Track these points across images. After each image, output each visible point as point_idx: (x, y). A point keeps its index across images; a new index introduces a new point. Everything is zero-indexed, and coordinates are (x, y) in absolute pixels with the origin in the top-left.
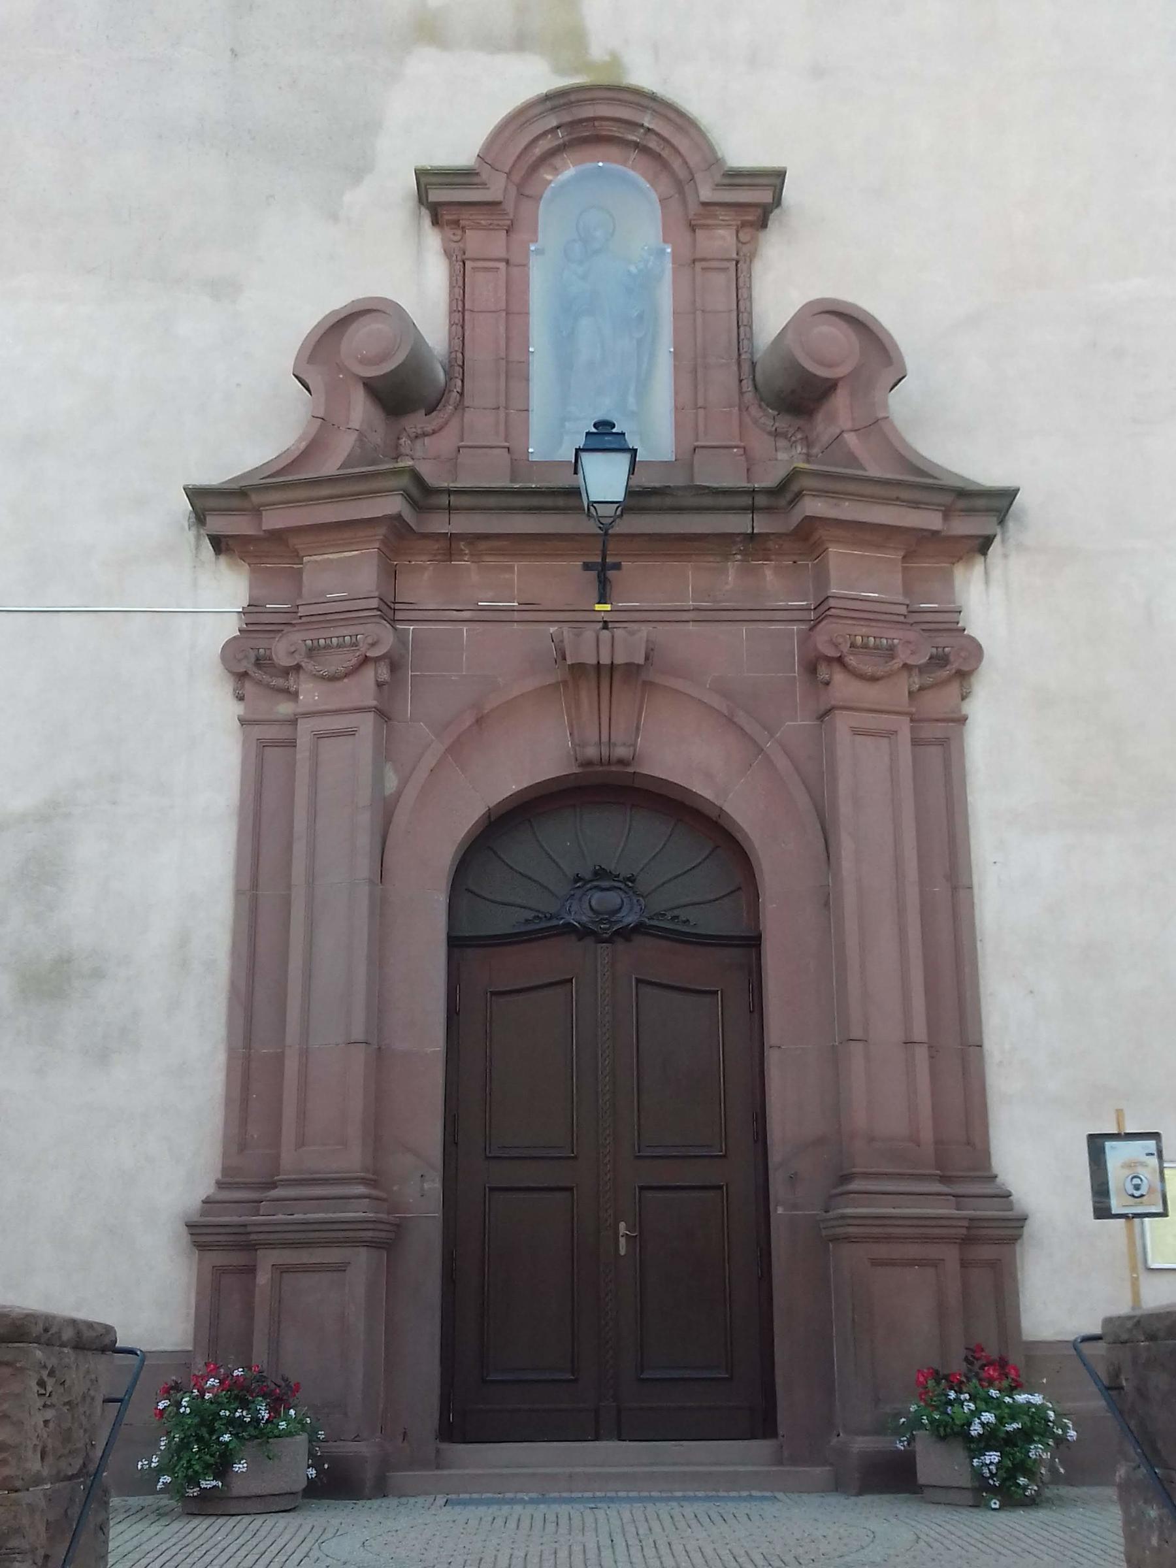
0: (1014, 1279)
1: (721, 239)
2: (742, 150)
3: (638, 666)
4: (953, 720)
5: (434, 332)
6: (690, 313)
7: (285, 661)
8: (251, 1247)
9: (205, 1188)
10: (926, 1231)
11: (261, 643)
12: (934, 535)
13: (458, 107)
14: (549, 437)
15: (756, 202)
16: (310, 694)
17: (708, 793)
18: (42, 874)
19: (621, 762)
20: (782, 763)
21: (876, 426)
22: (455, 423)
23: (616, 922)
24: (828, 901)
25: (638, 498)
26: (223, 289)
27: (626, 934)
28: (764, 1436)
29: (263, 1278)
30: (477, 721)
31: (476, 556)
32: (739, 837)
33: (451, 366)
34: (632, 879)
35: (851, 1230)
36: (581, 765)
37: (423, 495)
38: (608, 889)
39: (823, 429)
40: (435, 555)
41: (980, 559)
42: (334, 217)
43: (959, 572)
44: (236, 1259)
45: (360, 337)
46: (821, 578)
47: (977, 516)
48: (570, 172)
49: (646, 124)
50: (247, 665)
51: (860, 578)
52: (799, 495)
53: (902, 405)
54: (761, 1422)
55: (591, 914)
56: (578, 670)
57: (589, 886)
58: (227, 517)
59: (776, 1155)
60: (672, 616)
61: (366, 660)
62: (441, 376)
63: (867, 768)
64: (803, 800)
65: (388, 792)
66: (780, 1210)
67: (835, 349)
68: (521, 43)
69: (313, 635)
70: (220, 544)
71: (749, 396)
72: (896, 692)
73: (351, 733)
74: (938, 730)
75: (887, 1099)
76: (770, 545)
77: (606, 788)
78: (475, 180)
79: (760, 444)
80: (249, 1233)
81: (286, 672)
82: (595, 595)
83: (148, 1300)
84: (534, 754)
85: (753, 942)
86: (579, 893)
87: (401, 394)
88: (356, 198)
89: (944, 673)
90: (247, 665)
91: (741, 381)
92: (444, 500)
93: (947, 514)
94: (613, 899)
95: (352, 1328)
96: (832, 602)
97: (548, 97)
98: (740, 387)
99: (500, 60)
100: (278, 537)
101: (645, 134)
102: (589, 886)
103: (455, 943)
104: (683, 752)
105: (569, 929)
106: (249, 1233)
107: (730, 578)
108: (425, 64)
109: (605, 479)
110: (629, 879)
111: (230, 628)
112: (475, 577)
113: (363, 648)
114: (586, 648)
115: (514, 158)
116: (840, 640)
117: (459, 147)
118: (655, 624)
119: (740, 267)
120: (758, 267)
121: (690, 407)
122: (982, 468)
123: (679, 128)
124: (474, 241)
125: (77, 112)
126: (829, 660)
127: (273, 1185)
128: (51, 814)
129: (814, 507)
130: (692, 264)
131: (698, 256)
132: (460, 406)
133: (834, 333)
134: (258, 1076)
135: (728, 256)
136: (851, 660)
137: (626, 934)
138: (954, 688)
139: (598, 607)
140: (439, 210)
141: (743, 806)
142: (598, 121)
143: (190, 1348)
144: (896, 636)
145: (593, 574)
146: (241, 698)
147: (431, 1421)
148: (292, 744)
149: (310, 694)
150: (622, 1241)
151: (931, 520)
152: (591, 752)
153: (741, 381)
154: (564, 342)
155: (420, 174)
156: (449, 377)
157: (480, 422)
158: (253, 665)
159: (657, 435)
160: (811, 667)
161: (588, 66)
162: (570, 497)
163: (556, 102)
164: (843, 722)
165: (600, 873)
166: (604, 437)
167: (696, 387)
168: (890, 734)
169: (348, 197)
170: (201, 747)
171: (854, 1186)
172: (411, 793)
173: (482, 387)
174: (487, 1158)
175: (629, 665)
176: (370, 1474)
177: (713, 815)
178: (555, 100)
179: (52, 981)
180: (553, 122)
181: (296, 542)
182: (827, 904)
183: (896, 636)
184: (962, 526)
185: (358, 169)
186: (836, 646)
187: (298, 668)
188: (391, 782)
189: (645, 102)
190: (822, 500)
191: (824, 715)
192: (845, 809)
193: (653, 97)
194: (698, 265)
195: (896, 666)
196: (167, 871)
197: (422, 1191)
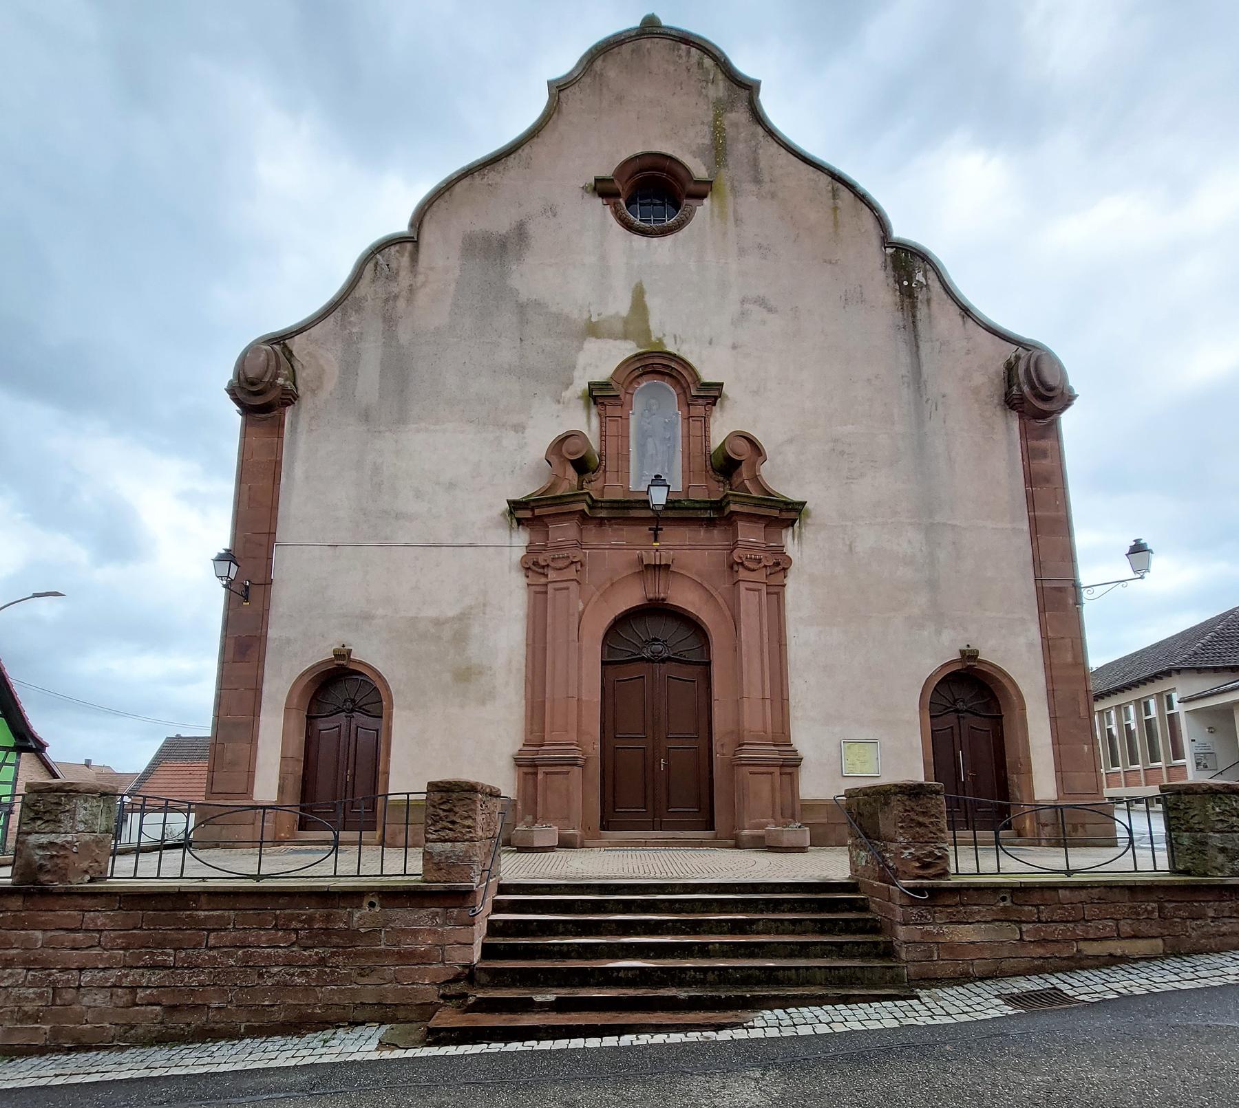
1: (698, 410)
2: (707, 376)
5: (595, 445)
6: (687, 436)
8: (536, 766)
9: (520, 747)
10: (769, 763)
11: (534, 557)
13: (603, 360)
14: (637, 484)
15: (712, 394)
16: (552, 575)
18: (461, 638)
19: (664, 600)
20: (720, 600)
21: (756, 479)
24: (736, 649)
25: (671, 505)
26: (519, 428)
27: (663, 661)
29: (540, 776)
31: (610, 525)
37: (594, 504)
39: (736, 480)
42: (559, 402)
43: (784, 531)
44: (530, 770)
45: (571, 445)
47: (787, 514)
48: (644, 384)
50: (530, 565)
51: (749, 534)
52: (728, 503)
53: (766, 471)
54: (710, 825)
56: (647, 566)
58: (525, 513)
59: (715, 738)
60: (680, 547)
63: (749, 602)
64: (728, 613)
68: (625, 336)
70: (520, 522)
71: (709, 467)
72: (761, 576)
74: (775, 589)
75: (755, 719)
77: (656, 610)
79: (713, 485)
81: (543, 567)
84: (631, 597)
87: (582, 466)
88: (567, 394)
90: (530, 565)
93: (781, 510)
95: (580, 792)
97: (636, 355)
99: (618, 342)
103: (603, 663)
104: (684, 597)
105: (642, 659)
107: (702, 534)
108: (592, 345)
109: (659, 497)
117: (603, 372)
119: (705, 419)
121: (688, 471)
122: (794, 495)
126: (738, 564)
128: (463, 617)
129: (733, 507)
130: (688, 418)
132: (605, 471)
133: (744, 446)
136: (746, 563)
137: (663, 661)
142: (658, 365)
144: (762, 555)
148: (546, 593)
149: (552, 575)
151: (775, 513)
152: (651, 596)
154: (642, 447)
155: (589, 384)
158: (532, 566)
159: (677, 485)
160: (731, 567)
161: (650, 343)
162: (645, 504)
164: (742, 586)
165: (655, 640)
166: (658, 480)
170: (512, 597)
173: (610, 464)
178: (639, 357)
183: (762, 555)
184: (785, 515)
185: (568, 384)
191: (736, 583)
193: (675, 355)
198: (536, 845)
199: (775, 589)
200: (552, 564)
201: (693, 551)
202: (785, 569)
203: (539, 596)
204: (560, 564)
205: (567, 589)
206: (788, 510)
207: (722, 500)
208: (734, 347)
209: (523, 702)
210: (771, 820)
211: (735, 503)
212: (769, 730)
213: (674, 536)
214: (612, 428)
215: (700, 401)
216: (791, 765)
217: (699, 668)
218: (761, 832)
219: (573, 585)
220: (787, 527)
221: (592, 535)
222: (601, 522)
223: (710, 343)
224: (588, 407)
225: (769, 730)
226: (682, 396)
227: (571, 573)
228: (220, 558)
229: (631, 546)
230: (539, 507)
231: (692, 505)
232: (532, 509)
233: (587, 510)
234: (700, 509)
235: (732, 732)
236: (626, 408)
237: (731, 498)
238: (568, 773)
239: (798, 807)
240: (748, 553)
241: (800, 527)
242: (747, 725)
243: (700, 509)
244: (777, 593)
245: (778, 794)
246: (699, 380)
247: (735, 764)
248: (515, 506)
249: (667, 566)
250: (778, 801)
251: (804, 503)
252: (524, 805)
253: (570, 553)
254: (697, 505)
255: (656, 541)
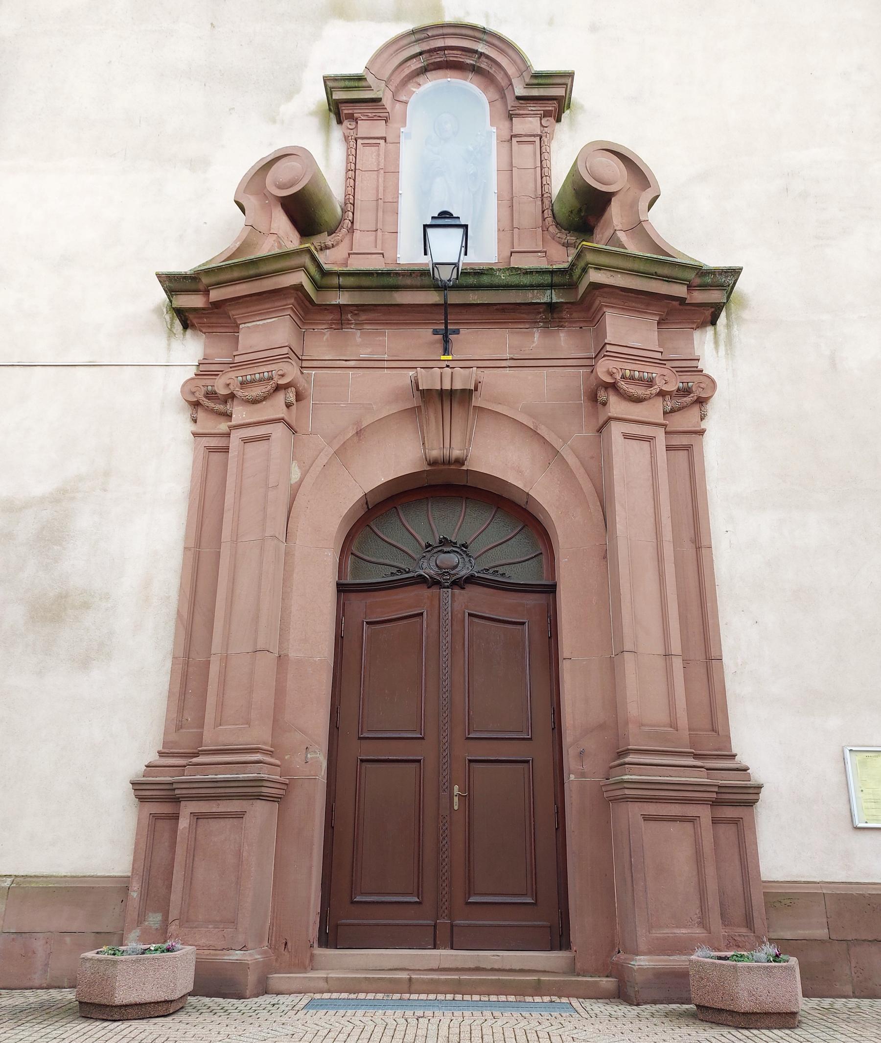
0: (754, 833)
1: (529, 124)
3: (470, 391)
4: (695, 432)
6: (509, 170)
7: (222, 391)
8: (176, 800)
9: (152, 757)
10: (684, 795)
12: (682, 300)
13: (354, 47)
15: (550, 98)
16: (240, 413)
17: (520, 485)
18: (52, 538)
19: (460, 462)
20: (572, 460)
21: (638, 229)
22: (347, 241)
23: (455, 574)
24: (606, 555)
28: (561, 949)
29: (184, 823)
30: (357, 433)
31: (359, 324)
32: (541, 517)
33: (346, 204)
34: (465, 546)
35: (627, 792)
36: (429, 464)
37: (324, 278)
38: (448, 552)
40: (331, 324)
41: (710, 330)
43: (697, 335)
46: (601, 333)
47: (698, 297)
49: (480, 50)
50: (200, 396)
51: (626, 330)
52: (585, 270)
54: (559, 939)
55: (437, 569)
57: (435, 550)
58: (201, 301)
59: (568, 738)
60: (493, 364)
61: (278, 388)
62: (339, 210)
63: (632, 463)
64: (587, 486)
65: (293, 481)
66: (572, 777)
67: (610, 175)
69: (243, 373)
71: (550, 220)
72: (653, 411)
73: (266, 438)
74: (684, 440)
75: (649, 697)
76: (565, 314)
77: (444, 485)
78: (363, 84)
80: (174, 789)
82: (441, 351)
83: (98, 840)
84: (398, 457)
85: (551, 589)
86: (428, 555)
88: (289, 109)
89: (688, 399)
90: (200, 396)
91: (543, 212)
92: (335, 281)
93: (690, 287)
94: (454, 558)
95: (270, 861)
96: (608, 348)
97: (413, 32)
98: (543, 216)
100: (217, 305)
101: (479, 58)
102: (435, 550)
103: (342, 589)
104: (497, 456)
105: (421, 580)
106: (174, 789)
107: (536, 341)
110: (463, 545)
111: (191, 373)
112: (359, 340)
113: (276, 378)
114: (430, 380)
115: (391, 71)
116: (615, 371)
118: (482, 370)
119: (541, 139)
120: (554, 146)
121: (509, 228)
123: (502, 51)
124: (365, 128)
125: (110, 62)
127: (196, 755)
128: (62, 497)
129: (595, 276)
131: (515, 132)
132: (351, 230)
134: (192, 676)
135: (535, 133)
136: (623, 385)
137: (459, 583)
138: (695, 411)
139: (443, 358)
140: (340, 105)
141: (544, 490)
143: (130, 874)
144: (654, 371)
145: (439, 337)
146: (195, 421)
147: (313, 932)
148: (226, 450)
150: (456, 799)
151: (679, 290)
152: (435, 453)
153: (543, 212)
156: (344, 211)
157: (363, 241)
158: (206, 401)
160: (593, 398)
163: (418, 36)
164: (616, 430)
165: (444, 542)
167: (493, 45)
168: (649, 439)
169: (283, 108)
170: (165, 453)
171: (630, 759)
172: (308, 480)
173: (364, 219)
174: (360, 738)
175: (463, 390)
176: (252, 978)
177: (522, 503)
179: (54, 611)
180: (417, 49)
181: (234, 313)
182: (605, 557)
183: (654, 371)
184: (699, 297)
186: (611, 374)
187: (232, 396)
188: (296, 475)
189: (477, 34)
190: (603, 279)
192: (618, 489)
193: (484, 31)
194: (514, 140)
195: (654, 392)
196: (140, 540)
197: (312, 761)
198: (122, 997)
199: (684, 440)
200: (239, 393)
201: (520, 378)
202: (701, 402)
203: (214, 451)
204: (256, 392)
205: (266, 438)
206: (704, 287)
207: (573, 265)
208: (594, 28)
209: (168, 664)
210: (698, 932)
211: (599, 268)
212: (683, 721)
213: (478, 343)
214: (368, 157)
215: (532, 107)
216: (735, 800)
217: (531, 600)
218: (677, 961)
219: (278, 432)
220: (702, 325)
221: (322, 344)
222: (341, 316)
223: (551, 22)
224: (327, 128)
225: (683, 721)
226: (499, 104)
227: (276, 407)
228: (760, 787)
229: (398, 363)
230: (219, 284)
231: (515, 280)
232: (206, 292)
233: (308, 287)
234: (532, 287)
235: (602, 727)
236: (393, 125)
237: (590, 257)
238: (239, 816)
239: (758, 900)
240: (629, 367)
241: (728, 326)
242: (633, 710)
243: (532, 287)
244: (688, 448)
245: (710, 871)
246: (528, 67)
247: (610, 798)
248: (174, 284)
249: (466, 395)
250: (712, 887)
251: (735, 272)
252: (146, 895)
253: (276, 368)
254: (526, 280)
255: (446, 351)
